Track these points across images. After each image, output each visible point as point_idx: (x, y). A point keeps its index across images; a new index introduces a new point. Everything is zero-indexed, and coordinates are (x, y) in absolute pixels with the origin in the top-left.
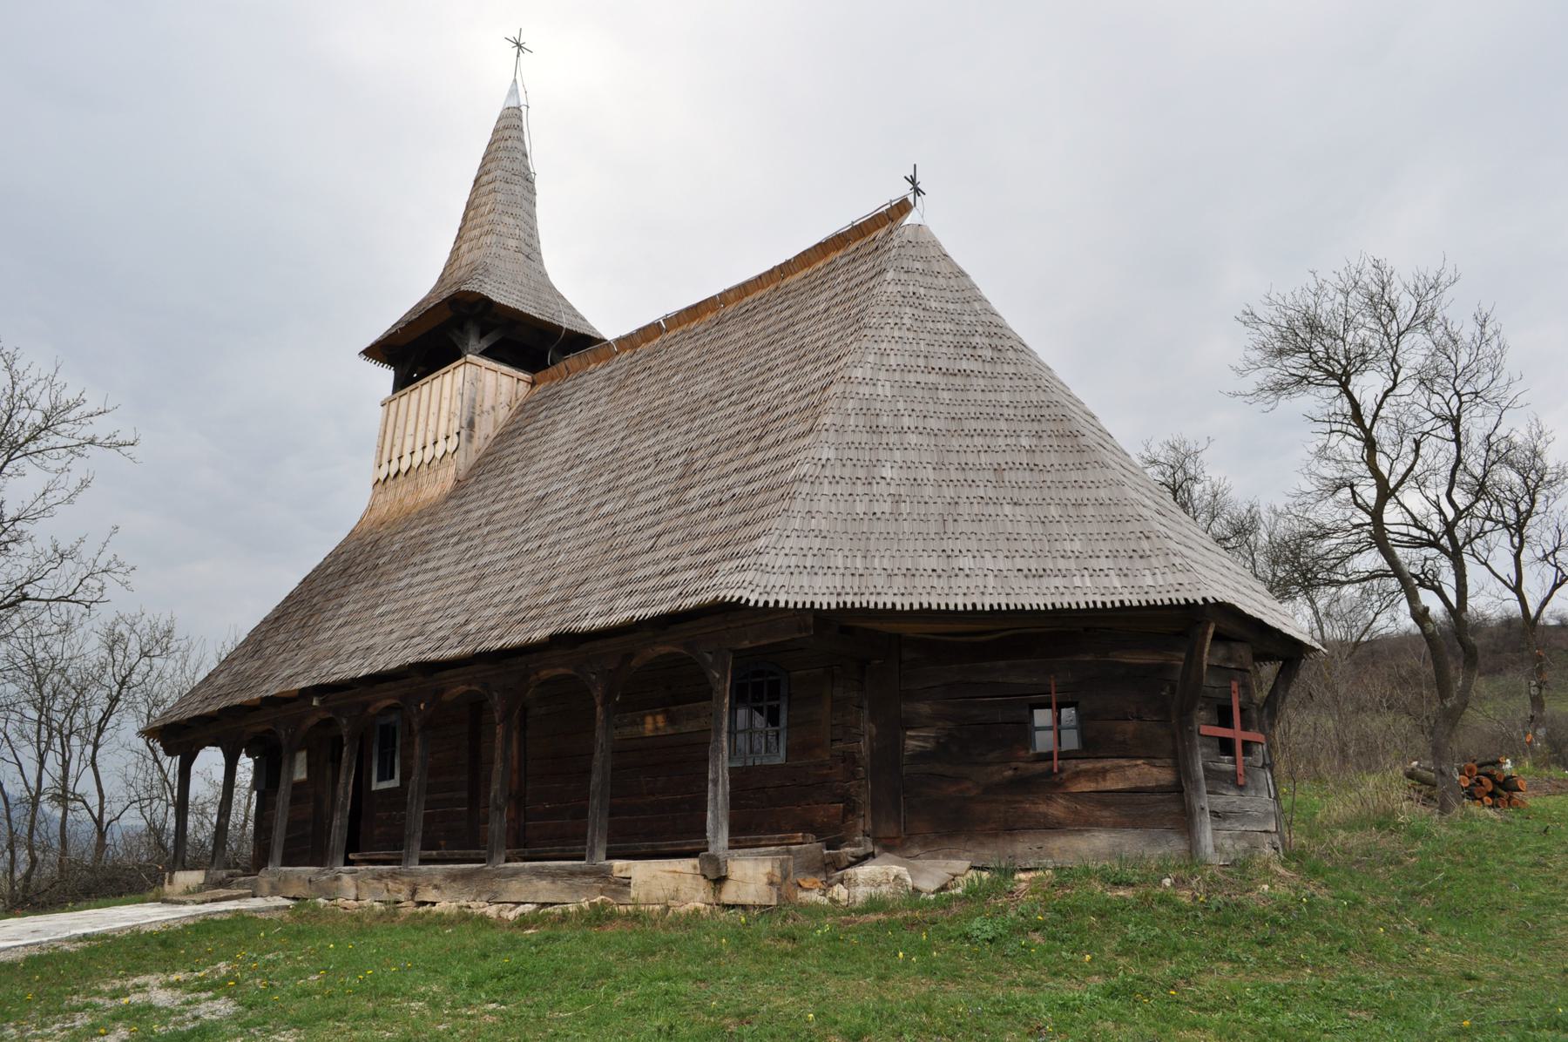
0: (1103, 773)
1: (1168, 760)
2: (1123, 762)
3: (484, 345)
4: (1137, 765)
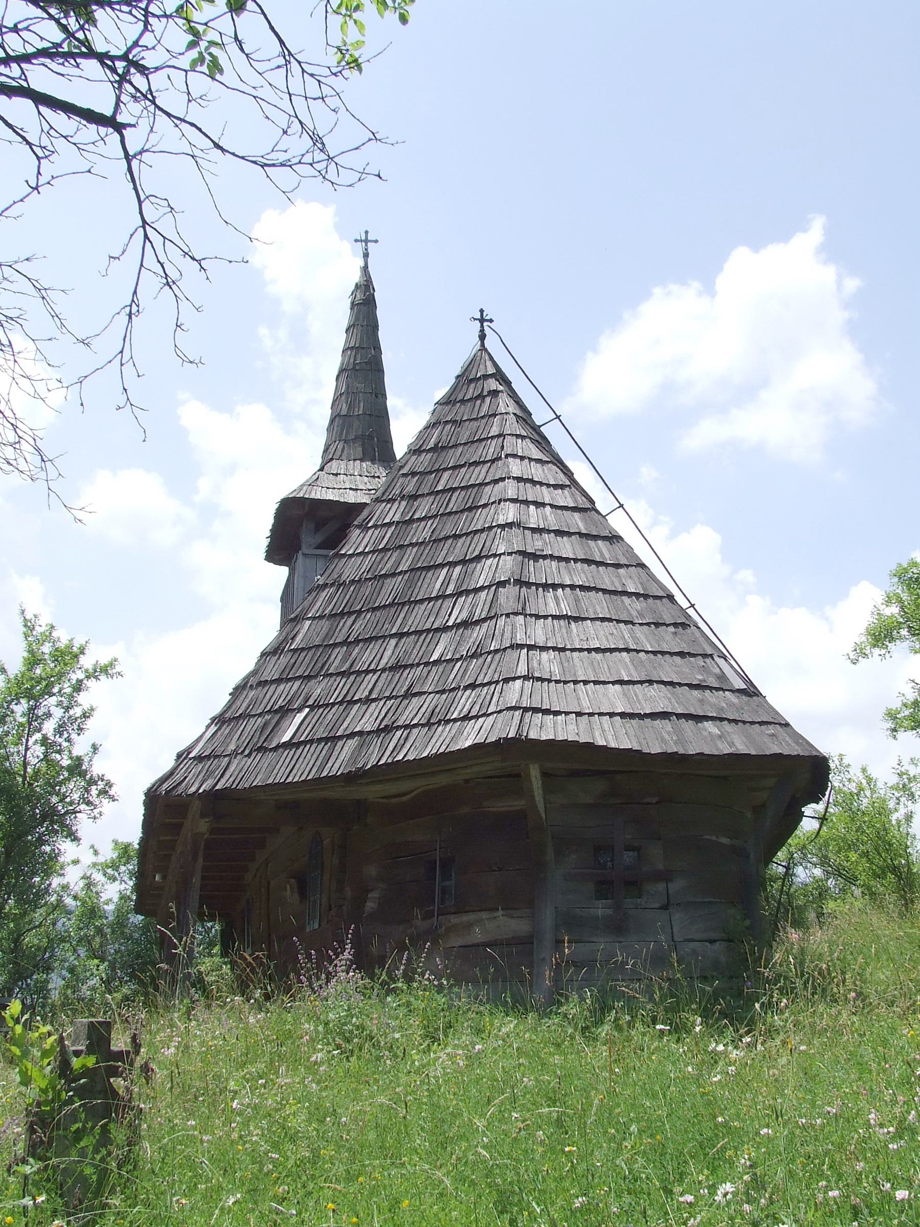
0: (469, 926)
1: (526, 910)
2: (484, 915)
3: (319, 538)
4: (495, 918)
